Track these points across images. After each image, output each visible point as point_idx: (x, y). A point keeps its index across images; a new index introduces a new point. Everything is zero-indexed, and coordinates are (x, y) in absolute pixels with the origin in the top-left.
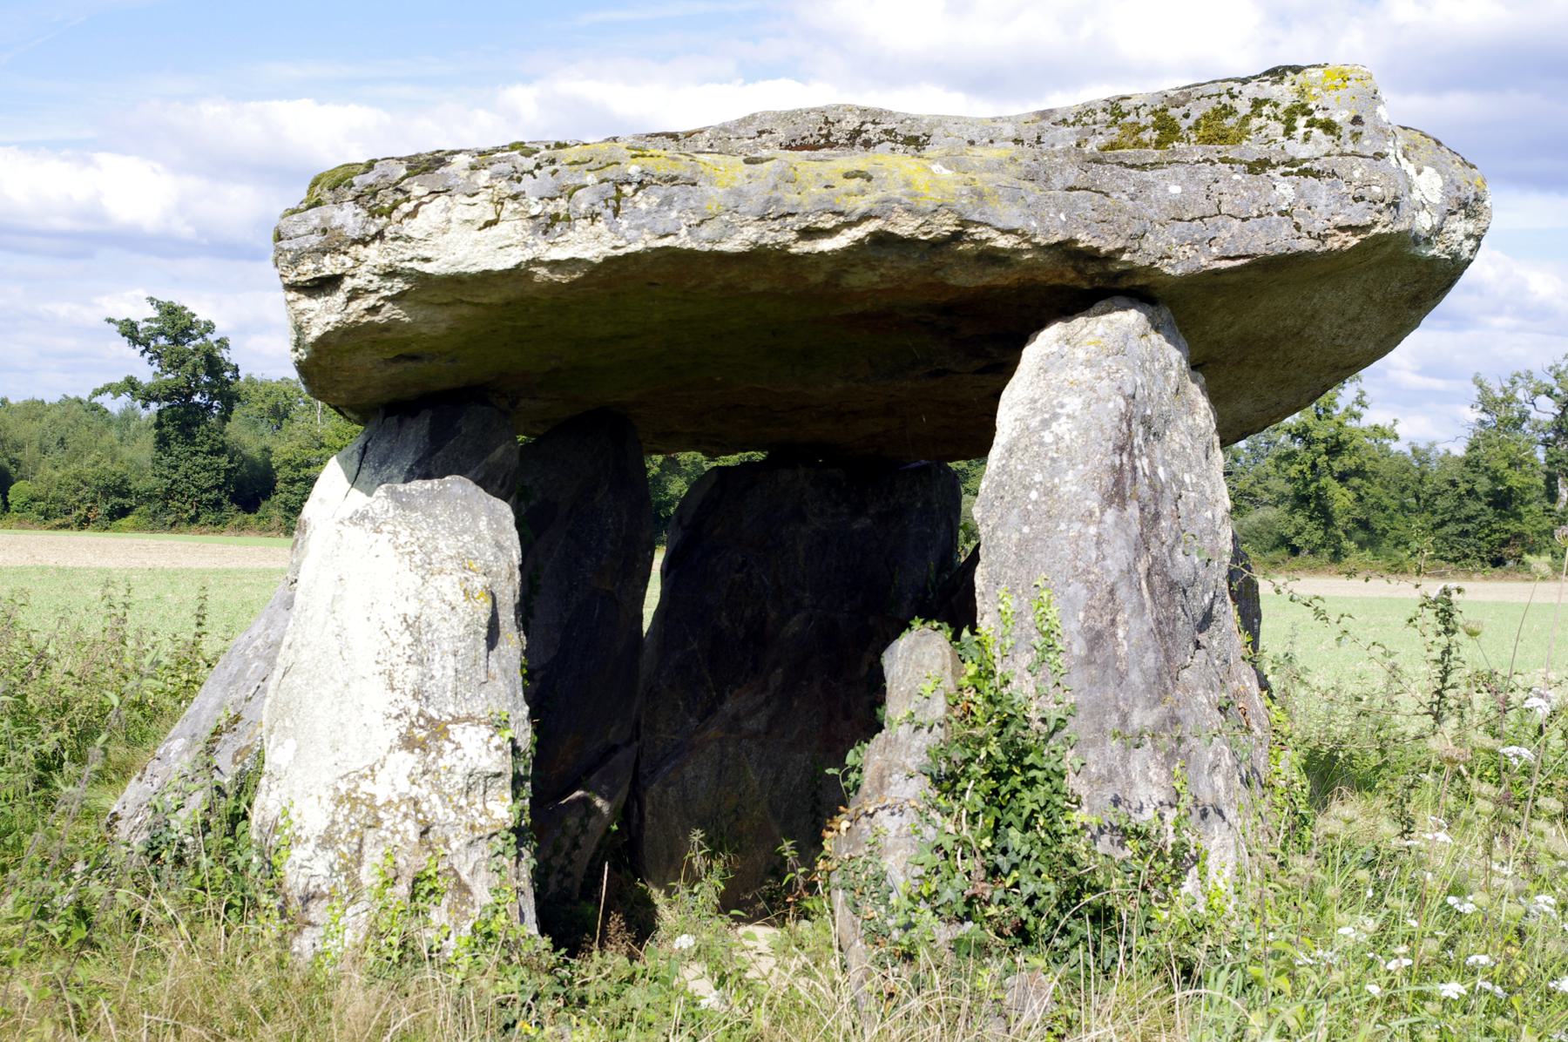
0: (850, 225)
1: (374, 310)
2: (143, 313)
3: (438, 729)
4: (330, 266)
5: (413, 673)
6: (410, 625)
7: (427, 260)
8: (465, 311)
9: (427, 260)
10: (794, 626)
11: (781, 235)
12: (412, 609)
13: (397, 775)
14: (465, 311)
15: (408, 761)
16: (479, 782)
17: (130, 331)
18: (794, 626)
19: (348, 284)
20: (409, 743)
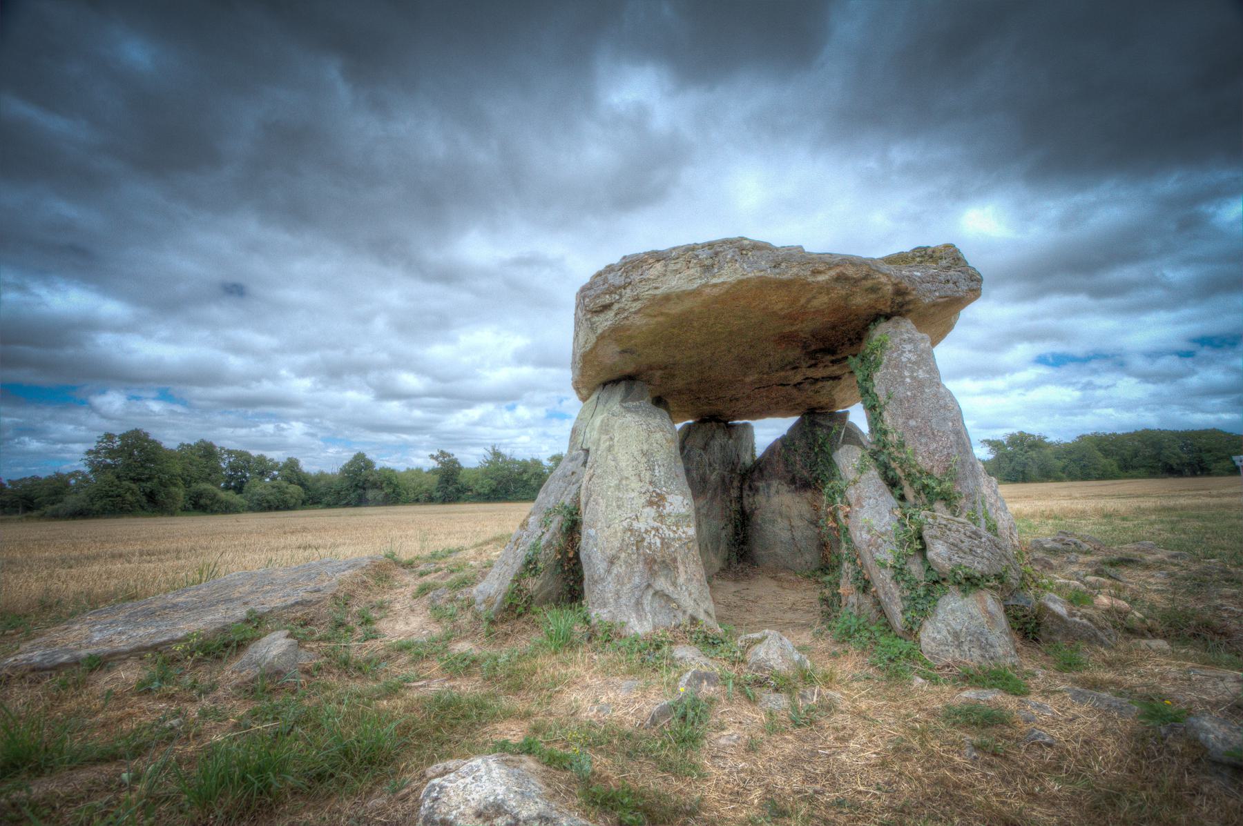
0: (830, 268)
1: (627, 318)
2: (435, 453)
3: (661, 498)
4: (607, 299)
5: (648, 474)
6: (644, 454)
7: (656, 288)
8: (661, 319)
9: (656, 288)
10: (713, 477)
11: (805, 273)
12: (645, 447)
13: (647, 519)
14: (661, 319)
15: (651, 511)
16: (680, 520)
17: (432, 456)
18: (713, 477)
19: (616, 307)
20: (650, 503)
